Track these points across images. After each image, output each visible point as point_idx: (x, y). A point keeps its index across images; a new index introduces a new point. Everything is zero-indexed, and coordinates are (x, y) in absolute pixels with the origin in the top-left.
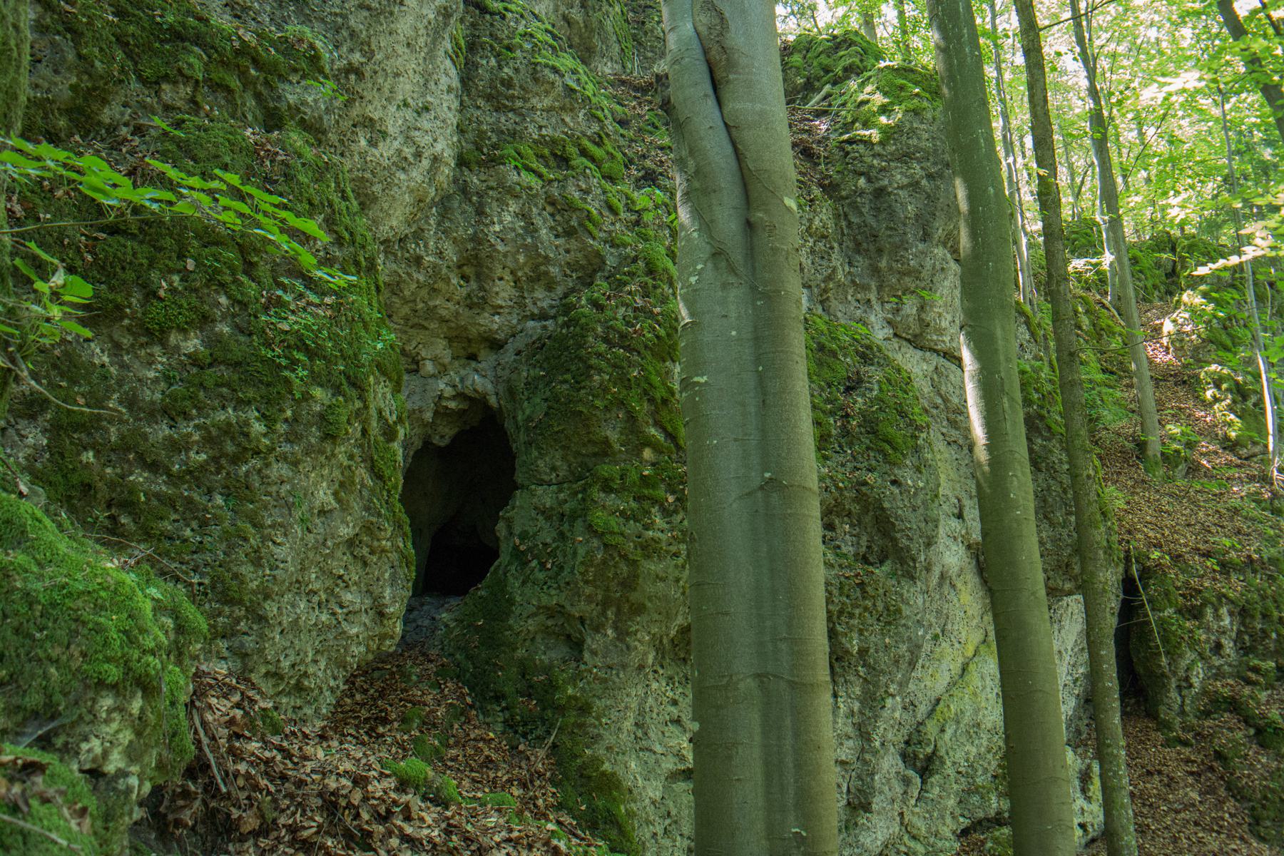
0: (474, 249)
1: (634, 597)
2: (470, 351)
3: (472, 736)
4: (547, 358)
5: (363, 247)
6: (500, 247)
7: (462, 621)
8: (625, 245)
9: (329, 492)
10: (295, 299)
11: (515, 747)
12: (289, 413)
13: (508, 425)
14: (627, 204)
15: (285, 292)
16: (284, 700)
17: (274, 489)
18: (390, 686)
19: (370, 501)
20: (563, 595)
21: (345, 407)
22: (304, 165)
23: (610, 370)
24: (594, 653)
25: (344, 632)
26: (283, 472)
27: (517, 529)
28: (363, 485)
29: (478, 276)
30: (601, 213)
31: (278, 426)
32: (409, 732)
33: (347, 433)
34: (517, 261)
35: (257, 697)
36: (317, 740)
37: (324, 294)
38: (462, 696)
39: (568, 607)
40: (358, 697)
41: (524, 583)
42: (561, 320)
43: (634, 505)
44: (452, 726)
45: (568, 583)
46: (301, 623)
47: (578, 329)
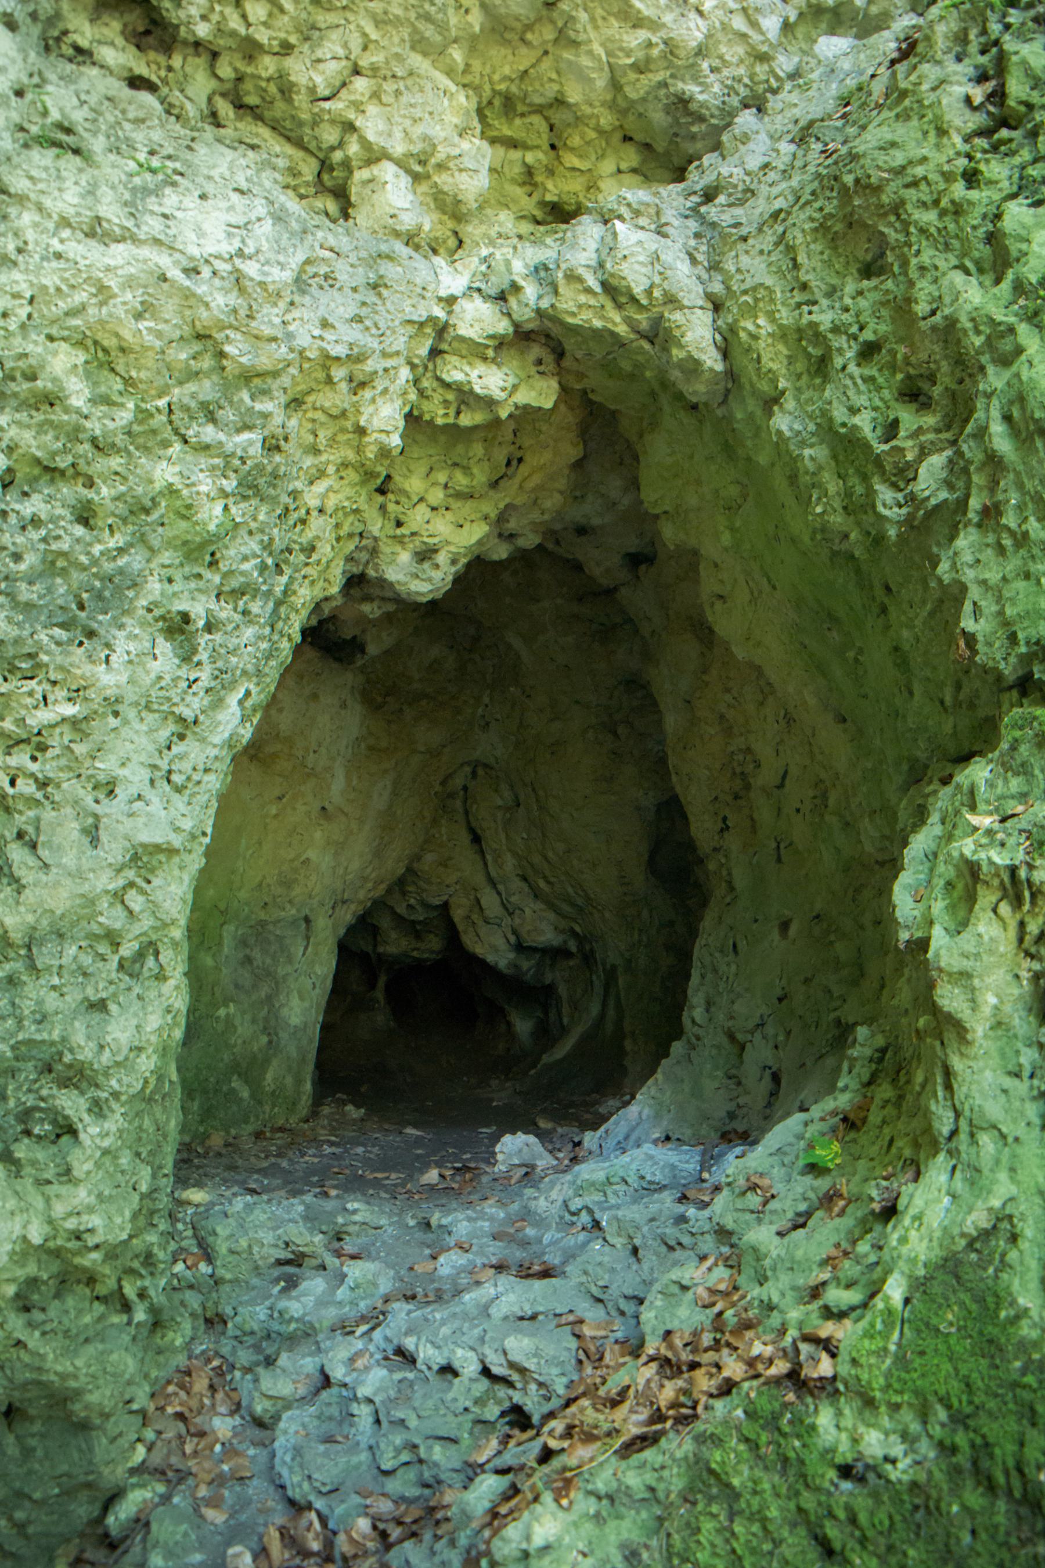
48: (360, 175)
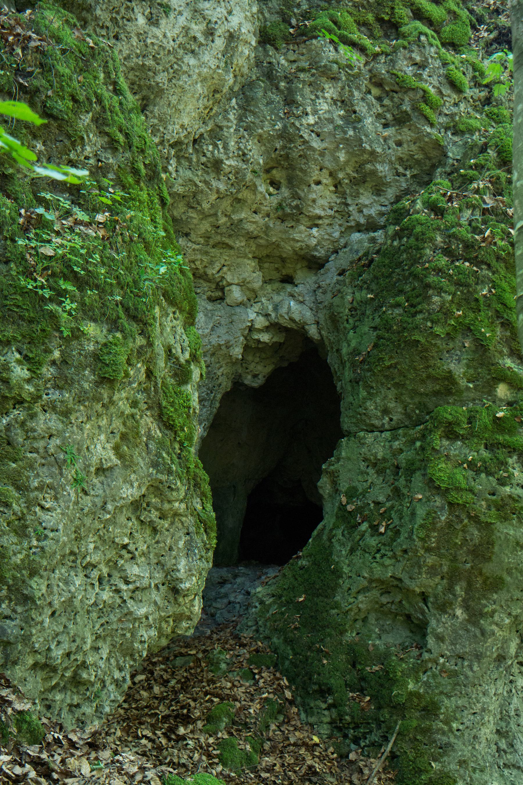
0: (284, 147)
1: (488, 568)
2: (284, 272)
3: (292, 740)
4: (376, 278)
5: (143, 151)
6: (316, 144)
7: (280, 597)
8: (471, 131)
9: (108, 446)
10: (60, 218)
11: (343, 756)
12: (57, 354)
13: (332, 360)
14: (474, 77)
15: (47, 209)
16: (59, 697)
17: (41, 444)
18: (195, 675)
19: (159, 455)
20: (400, 566)
21: (124, 345)
22: (63, 52)
23: (453, 289)
24: (440, 639)
25: (130, 613)
26: (51, 424)
27: (344, 486)
28: (149, 437)
29: (291, 181)
30: (440, 93)
31: (44, 370)
32: (216, 733)
33: (127, 375)
34: (336, 159)
35: (12, 697)
36: (86, 749)
37: (95, 210)
38: (280, 689)
39: (407, 581)
40: (157, 689)
41: (352, 551)
42: (392, 229)
43: (485, 454)
44: (268, 727)
45: (405, 551)
46: (77, 603)
47: (412, 240)
48: (227, 289)
